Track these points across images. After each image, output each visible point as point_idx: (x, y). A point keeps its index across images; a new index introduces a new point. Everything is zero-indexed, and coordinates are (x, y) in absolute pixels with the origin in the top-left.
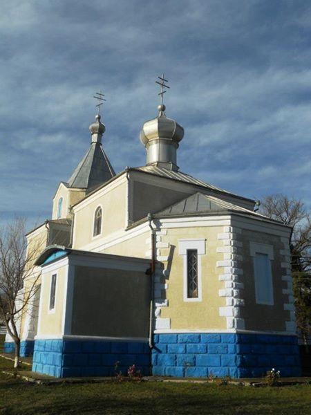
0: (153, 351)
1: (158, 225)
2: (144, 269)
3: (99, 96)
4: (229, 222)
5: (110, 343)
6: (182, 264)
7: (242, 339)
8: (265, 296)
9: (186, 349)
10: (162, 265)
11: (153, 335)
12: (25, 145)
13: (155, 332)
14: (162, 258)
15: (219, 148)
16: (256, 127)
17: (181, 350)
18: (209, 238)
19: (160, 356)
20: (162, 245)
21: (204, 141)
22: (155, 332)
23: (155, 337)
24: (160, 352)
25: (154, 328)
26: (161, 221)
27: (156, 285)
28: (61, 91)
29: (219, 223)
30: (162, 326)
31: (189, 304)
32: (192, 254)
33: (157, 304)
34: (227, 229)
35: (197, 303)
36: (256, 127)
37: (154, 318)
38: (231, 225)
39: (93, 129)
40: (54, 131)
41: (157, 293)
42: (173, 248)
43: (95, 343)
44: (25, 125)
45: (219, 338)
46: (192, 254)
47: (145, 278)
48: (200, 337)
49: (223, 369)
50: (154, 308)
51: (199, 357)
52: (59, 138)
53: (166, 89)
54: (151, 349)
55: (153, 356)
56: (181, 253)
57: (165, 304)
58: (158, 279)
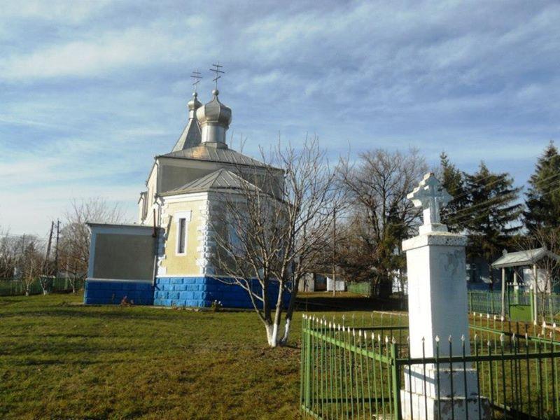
0: (156, 289)
1: (163, 201)
2: (152, 232)
3: (216, 68)
4: (206, 197)
5: (122, 284)
6: (176, 228)
7: (209, 281)
8: (237, 248)
9: (174, 288)
10: (164, 230)
11: (156, 278)
12: (239, 88)
13: (157, 276)
14: (164, 226)
15: (463, 68)
16: (510, 37)
17: (171, 288)
18: (190, 211)
19: (159, 292)
20: (165, 217)
21: (444, 62)
22: (157, 276)
23: (157, 280)
24: (159, 289)
25: (156, 274)
26: (164, 198)
27: (160, 245)
28: (270, 24)
29: (200, 198)
30: (162, 273)
31: (179, 258)
32: (183, 221)
33: (159, 258)
34: (205, 202)
35: (184, 257)
36: (510, 37)
37: (157, 267)
38: (208, 199)
39: (190, 106)
40: (267, 70)
41: (160, 250)
42: (171, 217)
43: (110, 283)
44: (237, 67)
45: (194, 280)
46: (183, 221)
47: (152, 240)
48: (183, 280)
49: (194, 300)
50: (157, 260)
51: (181, 293)
52: (273, 77)
53: (220, 74)
54: (153, 287)
55: (155, 292)
56: (176, 222)
57: (164, 257)
58: (160, 240)
